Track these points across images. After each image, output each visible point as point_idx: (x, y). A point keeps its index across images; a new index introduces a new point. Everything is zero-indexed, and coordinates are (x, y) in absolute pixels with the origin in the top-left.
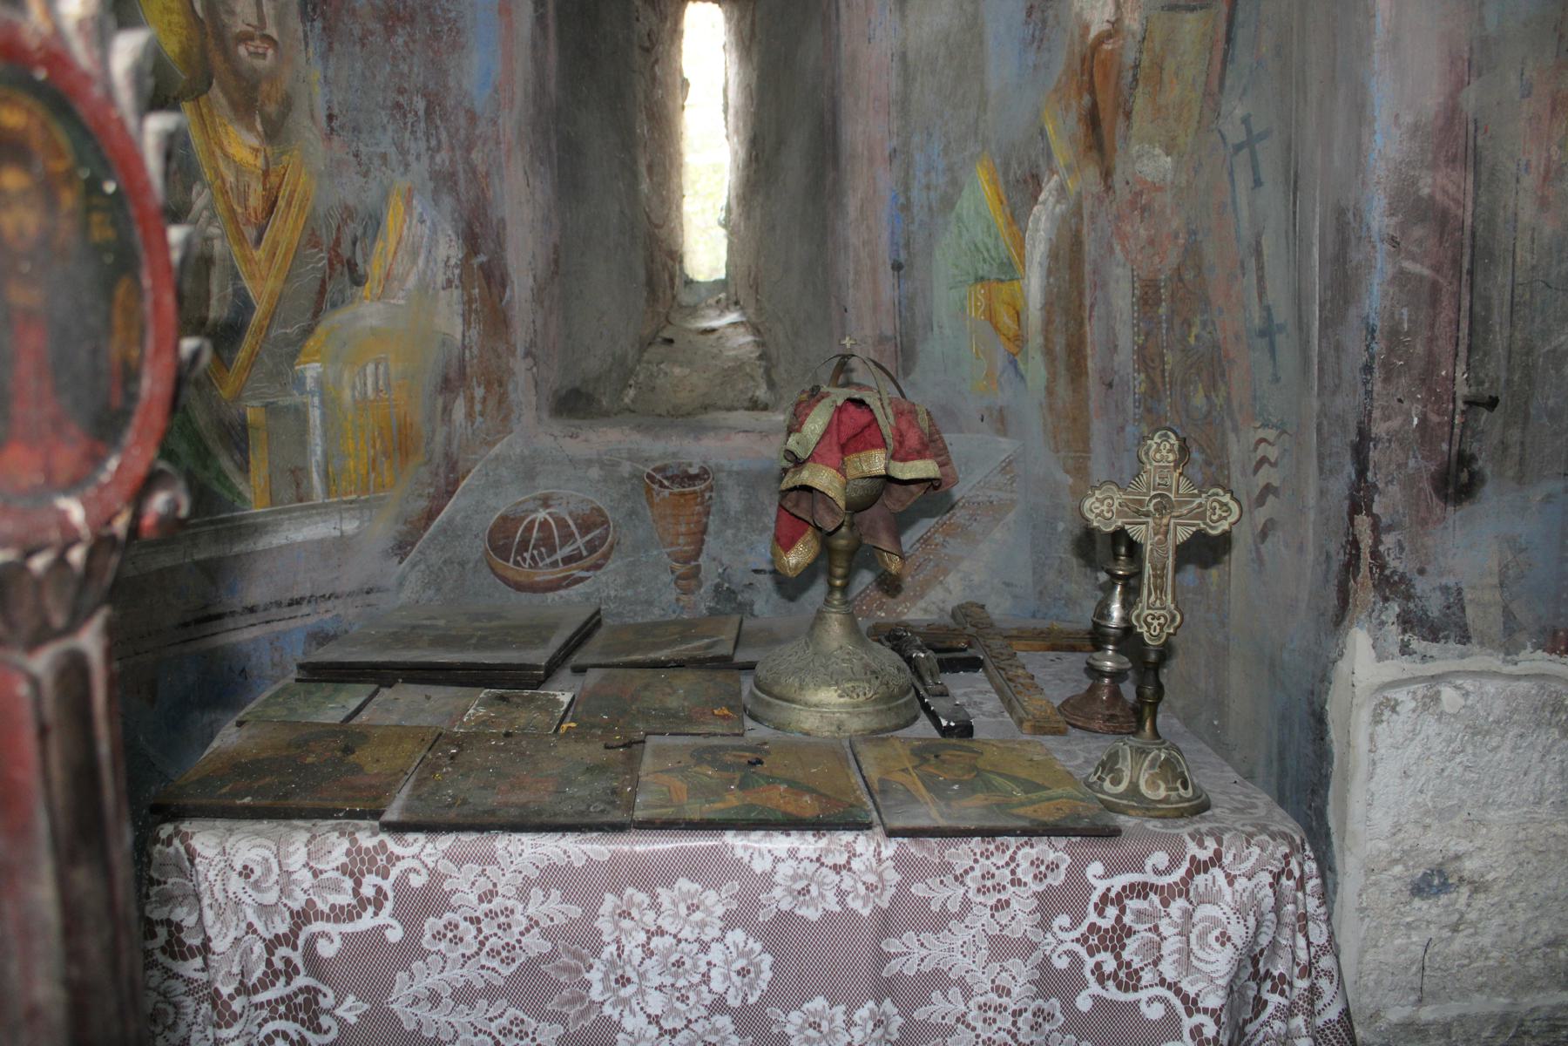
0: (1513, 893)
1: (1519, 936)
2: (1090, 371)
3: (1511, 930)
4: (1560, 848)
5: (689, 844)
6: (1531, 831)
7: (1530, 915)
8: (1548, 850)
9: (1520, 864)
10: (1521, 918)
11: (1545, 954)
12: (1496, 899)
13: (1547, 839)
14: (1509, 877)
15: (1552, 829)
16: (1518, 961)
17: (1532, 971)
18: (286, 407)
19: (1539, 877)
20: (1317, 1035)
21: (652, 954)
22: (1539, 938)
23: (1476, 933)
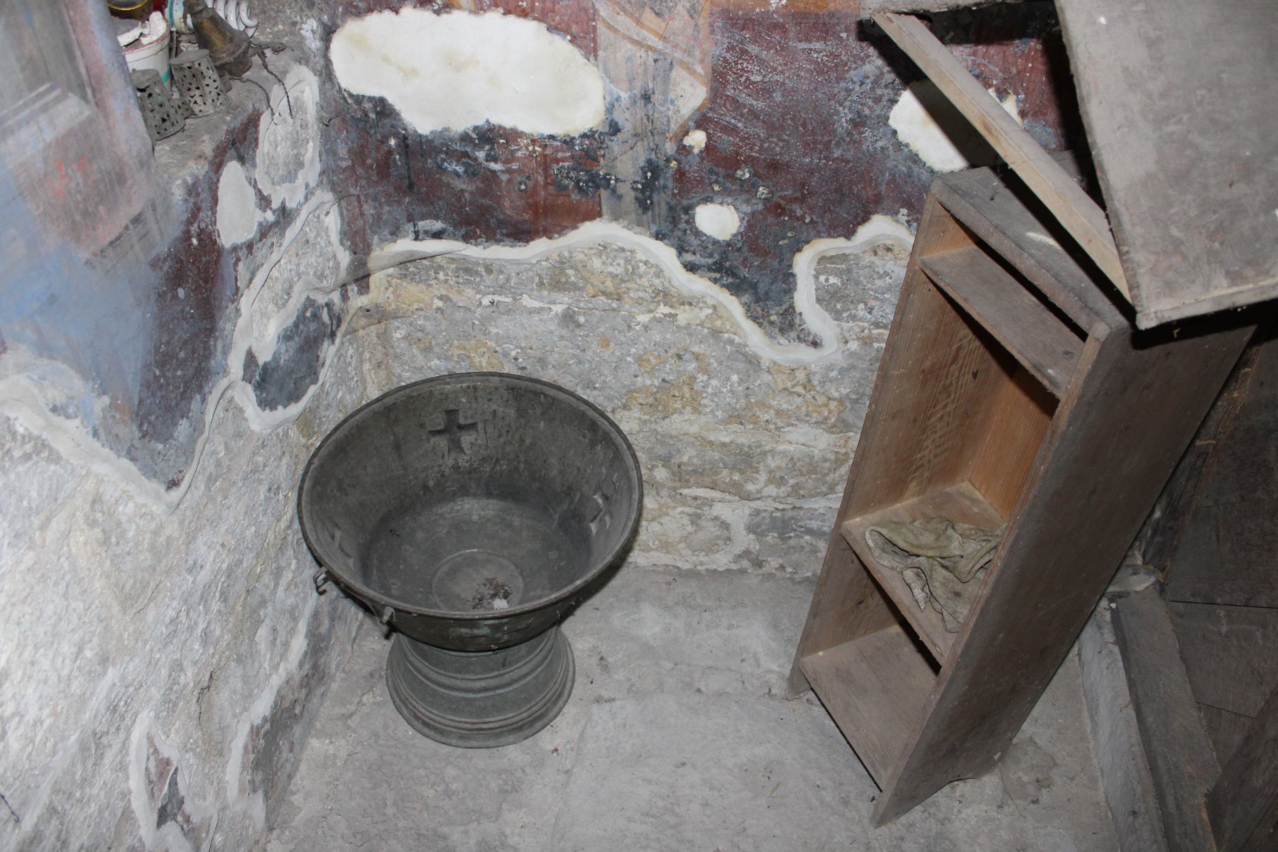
0: (27, 655)
1: (53, 679)
2: (1204, 810)
3: (45, 682)
4: (38, 575)
5: (402, 604)
6: (7, 587)
7: (51, 654)
8: (32, 588)
9: (19, 624)
10: (46, 664)
11: (79, 669)
12: (20, 673)
13: (24, 581)
14: (18, 645)
15: (22, 567)
16: (66, 697)
17: (78, 691)
18: (489, 495)
19: (39, 618)
20: (666, 2)
21: (943, 824)
22: (67, 661)
23: (22, 717)
